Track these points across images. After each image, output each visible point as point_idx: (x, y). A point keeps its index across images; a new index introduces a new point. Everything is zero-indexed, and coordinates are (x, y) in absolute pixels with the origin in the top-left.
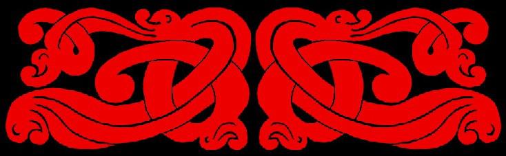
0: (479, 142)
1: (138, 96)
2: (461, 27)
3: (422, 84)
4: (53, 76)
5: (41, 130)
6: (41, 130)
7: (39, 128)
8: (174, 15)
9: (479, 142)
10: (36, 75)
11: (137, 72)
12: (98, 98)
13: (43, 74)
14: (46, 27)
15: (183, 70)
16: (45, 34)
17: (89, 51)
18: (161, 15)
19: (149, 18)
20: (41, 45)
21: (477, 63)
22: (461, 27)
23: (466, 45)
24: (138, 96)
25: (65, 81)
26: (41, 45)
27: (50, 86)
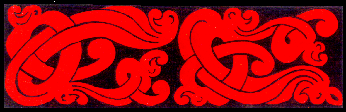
0: (309, 103)
1: (85, 43)
2: (313, 23)
3: (279, 67)
4: (145, 59)
5: (154, 19)
6: (154, 19)
7: (155, 21)
8: (60, 101)
9: (309, 103)
10: (157, 58)
11: (86, 61)
12: (113, 42)
13: (153, 58)
14: (150, 92)
15: (53, 61)
16: (151, 88)
17: (120, 76)
18: (69, 101)
19: (77, 98)
20: (154, 80)
21: (325, 52)
22: (313, 23)
23: (319, 39)
24: (85, 43)
25: (137, 54)
26: (154, 80)
27: (147, 51)
